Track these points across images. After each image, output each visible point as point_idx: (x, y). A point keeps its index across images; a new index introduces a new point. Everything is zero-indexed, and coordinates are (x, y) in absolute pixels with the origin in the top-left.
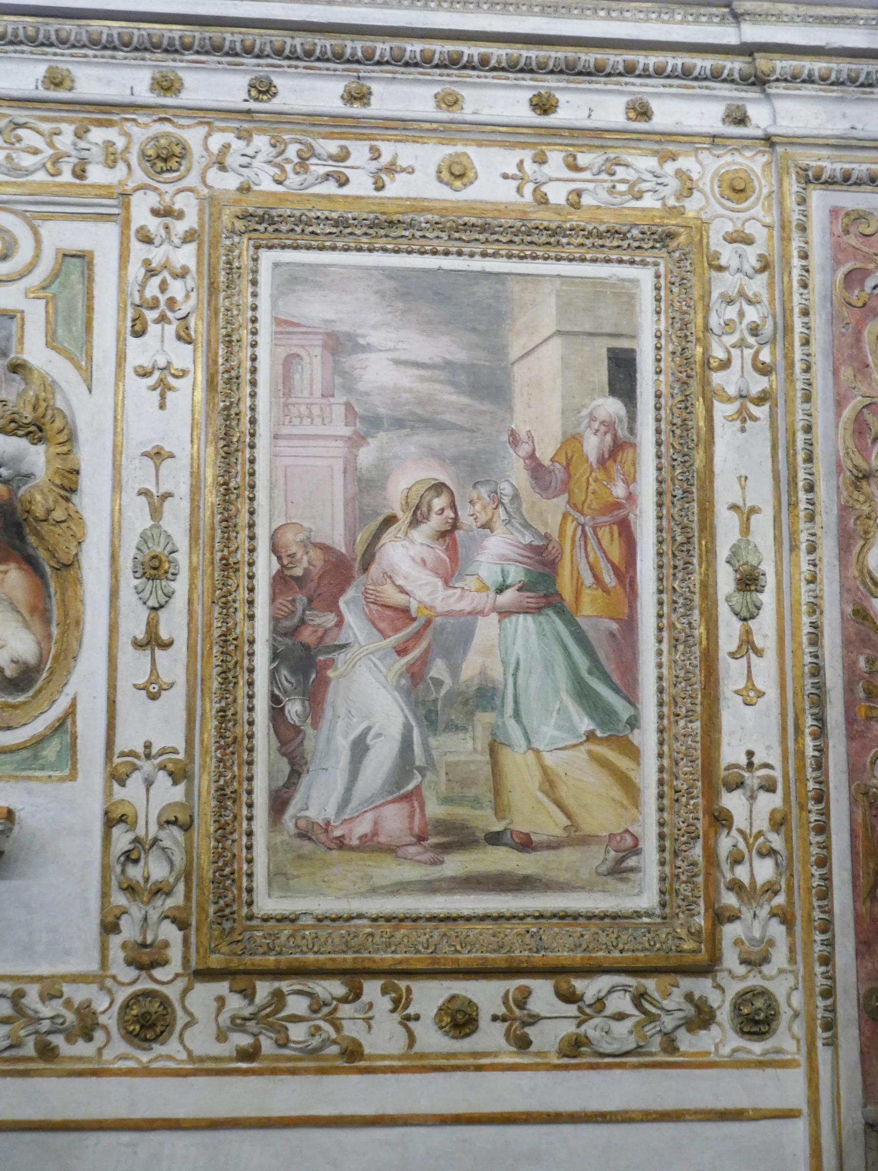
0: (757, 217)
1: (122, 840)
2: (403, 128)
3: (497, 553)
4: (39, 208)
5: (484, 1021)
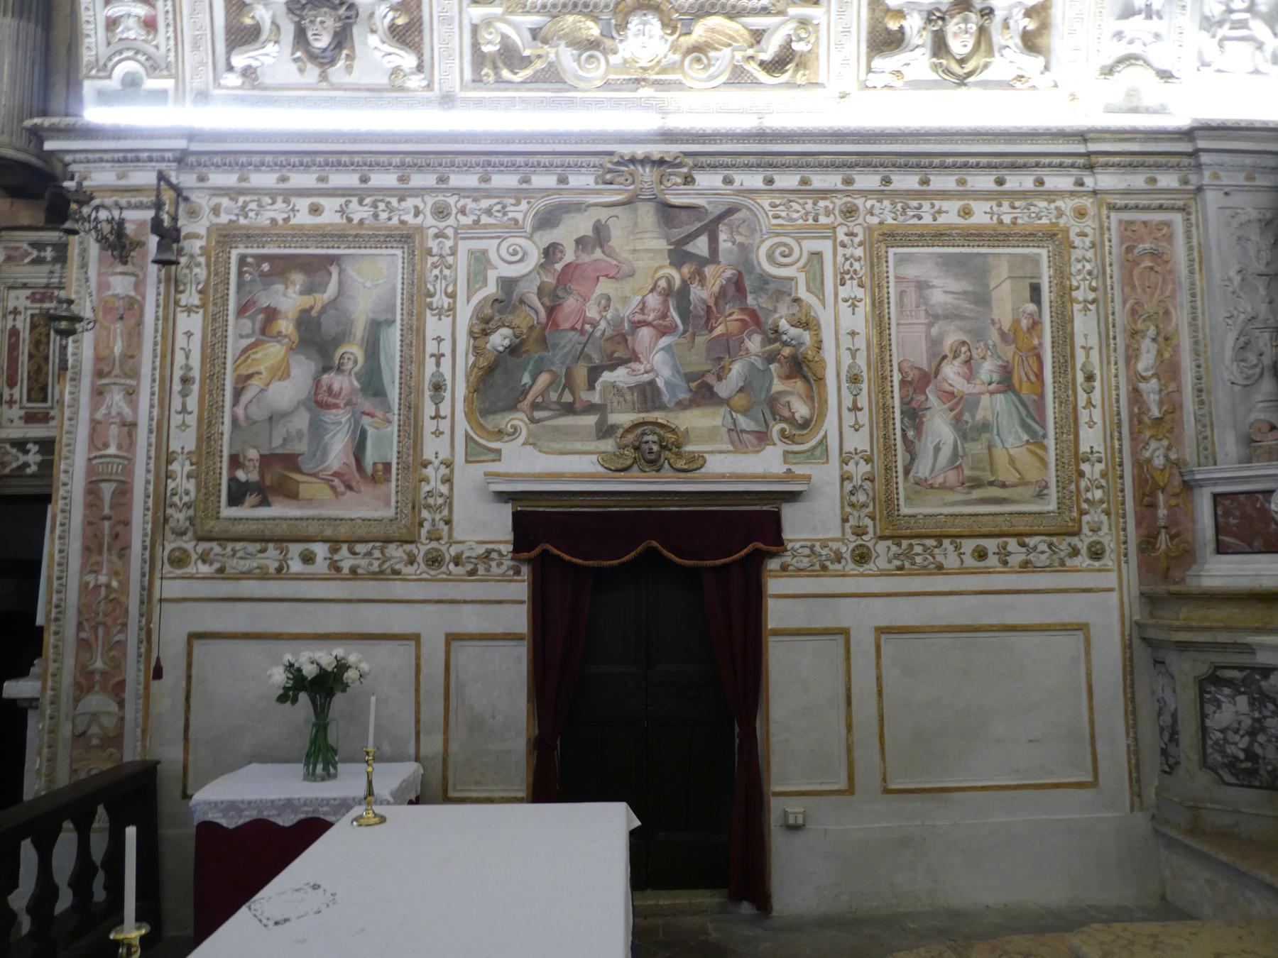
0: (1089, 225)
1: (848, 486)
2: (944, 195)
3: (988, 369)
4: (802, 234)
5: (990, 554)
